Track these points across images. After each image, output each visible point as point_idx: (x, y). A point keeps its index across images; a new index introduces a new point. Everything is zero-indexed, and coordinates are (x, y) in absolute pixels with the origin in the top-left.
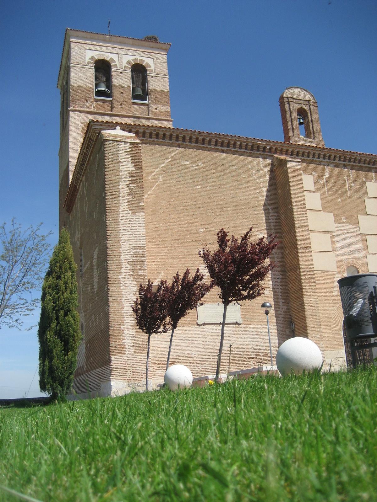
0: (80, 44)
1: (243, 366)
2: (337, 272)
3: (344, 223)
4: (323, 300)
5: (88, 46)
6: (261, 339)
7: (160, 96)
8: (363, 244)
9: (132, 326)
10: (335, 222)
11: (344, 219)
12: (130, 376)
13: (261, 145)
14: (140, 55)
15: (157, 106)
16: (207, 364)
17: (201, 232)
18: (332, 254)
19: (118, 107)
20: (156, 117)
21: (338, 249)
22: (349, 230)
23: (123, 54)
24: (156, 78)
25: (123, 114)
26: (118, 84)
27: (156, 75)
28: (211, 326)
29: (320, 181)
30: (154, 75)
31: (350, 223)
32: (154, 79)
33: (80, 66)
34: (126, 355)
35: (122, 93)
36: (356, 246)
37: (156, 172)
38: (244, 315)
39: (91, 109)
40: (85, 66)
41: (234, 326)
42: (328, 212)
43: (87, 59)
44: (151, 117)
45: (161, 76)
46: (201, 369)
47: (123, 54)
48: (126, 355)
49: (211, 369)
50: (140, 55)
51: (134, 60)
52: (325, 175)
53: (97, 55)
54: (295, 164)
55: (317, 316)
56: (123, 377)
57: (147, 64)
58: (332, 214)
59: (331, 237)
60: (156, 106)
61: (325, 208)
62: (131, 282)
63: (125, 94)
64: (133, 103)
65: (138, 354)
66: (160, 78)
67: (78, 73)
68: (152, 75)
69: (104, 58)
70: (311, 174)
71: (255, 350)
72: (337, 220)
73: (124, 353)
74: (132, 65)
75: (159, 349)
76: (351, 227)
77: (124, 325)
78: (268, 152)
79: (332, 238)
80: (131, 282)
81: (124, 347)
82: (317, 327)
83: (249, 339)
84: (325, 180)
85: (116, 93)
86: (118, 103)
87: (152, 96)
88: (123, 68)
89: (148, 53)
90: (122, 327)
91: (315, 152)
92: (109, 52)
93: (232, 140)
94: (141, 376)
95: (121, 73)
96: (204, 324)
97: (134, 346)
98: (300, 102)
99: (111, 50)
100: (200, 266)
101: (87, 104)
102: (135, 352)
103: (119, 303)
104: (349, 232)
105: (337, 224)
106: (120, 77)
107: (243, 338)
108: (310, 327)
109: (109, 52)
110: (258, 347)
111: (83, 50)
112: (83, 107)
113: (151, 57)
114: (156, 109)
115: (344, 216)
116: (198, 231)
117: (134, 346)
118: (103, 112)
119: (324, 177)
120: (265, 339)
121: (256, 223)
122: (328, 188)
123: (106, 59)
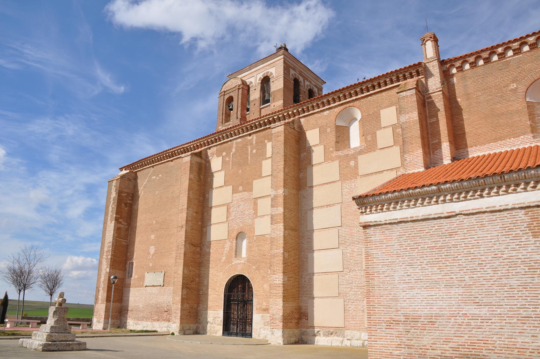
21: (232, 218)
27: (276, 79)
29: (227, 159)
51: (262, 76)
60: (274, 104)
76: (246, 194)
104: (244, 199)
115: (241, 185)
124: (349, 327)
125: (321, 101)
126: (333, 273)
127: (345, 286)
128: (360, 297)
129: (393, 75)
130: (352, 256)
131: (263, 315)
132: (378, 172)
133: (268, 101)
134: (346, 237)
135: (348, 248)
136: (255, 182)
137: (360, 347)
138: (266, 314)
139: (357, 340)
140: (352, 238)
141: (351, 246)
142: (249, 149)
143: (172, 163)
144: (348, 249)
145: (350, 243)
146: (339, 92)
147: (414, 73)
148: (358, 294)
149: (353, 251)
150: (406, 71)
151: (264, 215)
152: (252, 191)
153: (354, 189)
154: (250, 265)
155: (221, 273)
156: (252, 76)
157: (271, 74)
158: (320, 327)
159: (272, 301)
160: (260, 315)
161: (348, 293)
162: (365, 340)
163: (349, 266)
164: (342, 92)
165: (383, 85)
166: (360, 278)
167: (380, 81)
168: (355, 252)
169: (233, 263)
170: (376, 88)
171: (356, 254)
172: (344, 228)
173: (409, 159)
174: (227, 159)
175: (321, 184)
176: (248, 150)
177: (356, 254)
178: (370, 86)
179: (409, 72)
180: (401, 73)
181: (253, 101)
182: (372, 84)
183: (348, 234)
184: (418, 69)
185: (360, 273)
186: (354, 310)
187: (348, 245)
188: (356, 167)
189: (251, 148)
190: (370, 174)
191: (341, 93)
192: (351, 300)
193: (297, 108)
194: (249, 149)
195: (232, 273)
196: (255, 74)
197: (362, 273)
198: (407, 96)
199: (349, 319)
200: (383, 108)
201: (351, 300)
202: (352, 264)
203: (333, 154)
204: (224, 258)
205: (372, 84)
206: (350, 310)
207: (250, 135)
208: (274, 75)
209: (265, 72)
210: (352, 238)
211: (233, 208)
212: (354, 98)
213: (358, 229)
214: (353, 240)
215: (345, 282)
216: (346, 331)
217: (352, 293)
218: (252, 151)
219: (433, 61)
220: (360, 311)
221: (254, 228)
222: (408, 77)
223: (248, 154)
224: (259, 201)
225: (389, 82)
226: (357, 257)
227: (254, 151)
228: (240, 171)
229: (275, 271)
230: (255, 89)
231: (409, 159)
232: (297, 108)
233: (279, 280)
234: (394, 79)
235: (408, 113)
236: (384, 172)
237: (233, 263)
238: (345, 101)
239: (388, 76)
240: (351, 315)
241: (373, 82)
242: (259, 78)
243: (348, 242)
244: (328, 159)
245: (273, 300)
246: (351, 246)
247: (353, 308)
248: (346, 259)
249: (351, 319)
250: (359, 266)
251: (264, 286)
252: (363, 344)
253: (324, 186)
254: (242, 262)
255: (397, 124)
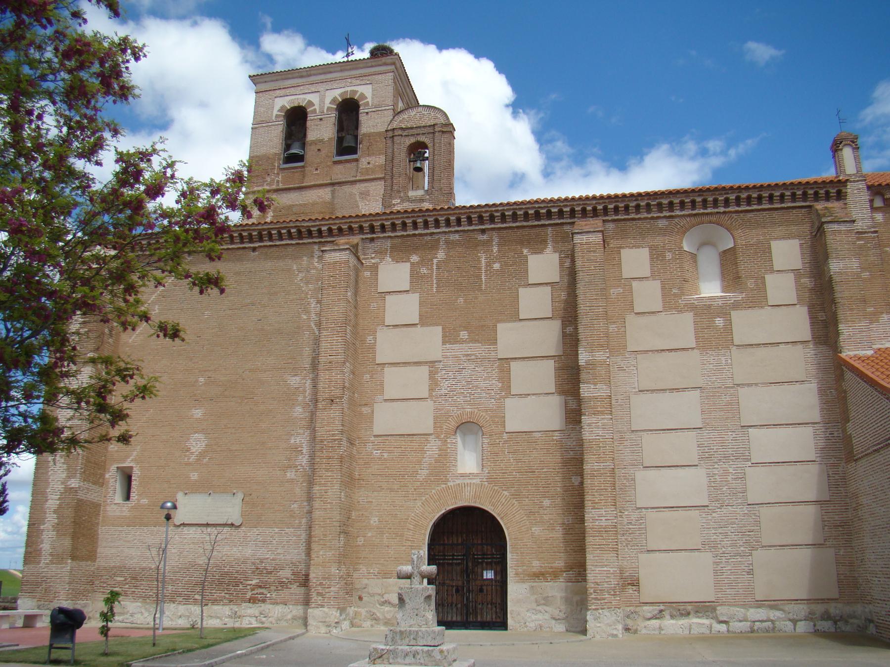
1: (235, 593)
2: (433, 436)
3: (463, 342)
4: (396, 487)
6: (270, 552)
7: (377, 141)
8: (500, 379)
9: (53, 526)
11: (464, 335)
12: (40, 595)
13: (312, 229)
14: (351, 85)
15: (370, 159)
16: (180, 585)
17: (201, 383)
18: (430, 403)
19: (312, 174)
21: (443, 391)
22: (472, 355)
24: (373, 113)
26: (314, 139)
27: (374, 110)
28: (194, 528)
29: (424, 271)
30: (370, 110)
31: (477, 341)
34: (41, 565)
35: (319, 150)
36: (482, 384)
37: (152, 300)
38: (248, 512)
39: (272, 185)
40: (270, 124)
41: (229, 529)
42: (431, 325)
43: (275, 112)
44: (360, 178)
45: (380, 109)
46: (170, 592)
48: (41, 565)
49: (185, 593)
50: (351, 85)
51: (341, 95)
53: (289, 102)
54: (338, 254)
55: (334, 520)
56: (34, 594)
58: (440, 328)
59: (430, 372)
60: (368, 159)
61: (425, 320)
62: (61, 465)
63: (324, 153)
64: (335, 163)
65: (54, 565)
66: (380, 112)
68: (366, 111)
70: (408, 260)
71: (257, 569)
72: (449, 338)
73: (39, 563)
75: (118, 558)
76: (478, 349)
77: (44, 524)
78: (308, 238)
79: (432, 375)
80: (61, 465)
81: (40, 555)
82: (330, 540)
83: (250, 552)
84: (435, 268)
85: (310, 153)
87: (365, 144)
88: (325, 111)
89: (364, 78)
90: (42, 527)
91: (414, 219)
93: (264, 230)
94: (53, 595)
96: (184, 525)
97: (51, 555)
98: (415, 131)
100: (192, 435)
101: (269, 179)
102: (52, 562)
103: (43, 494)
104: (473, 357)
105: (448, 346)
107: (240, 548)
108: (317, 539)
110: (263, 565)
112: (263, 185)
113: (368, 82)
114: (369, 163)
115: (466, 328)
116: (197, 381)
117: (51, 555)
119: (435, 261)
120: (276, 552)
121: (290, 361)
122: (438, 280)
123: (301, 104)
124: (724, 600)
125: (657, 201)
126: (687, 508)
127: (713, 532)
128: (742, 549)
129: (798, 189)
130: (726, 481)
131: (535, 584)
132: (770, 344)
133: (353, 150)
134: (712, 447)
135: (716, 466)
136: (500, 326)
137: (746, 632)
138: (540, 584)
139: (741, 621)
140: (724, 450)
141: (722, 463)
142: (483, 261)
143: (252, 253)
144: (717, 468)
145: (719, 458)
146: (684, 195)
147: (834, 193)
148: (738, 545)
149: (726, 472)
150: (821, 188)
151: (529, 395)
152: (496, 344)
153: (724, 367)
154: (496, 488)
155: (419, 503)
156: (313, 90)
157: (363, 96)
158: (666, 603)
159: (592, 558)
160: (526, 585)
161: (719, 542)
162: (754, 622)
163: (720, 498)
164: (702, 195)
165: (778, 200)
166: (743, 518)
167: (773, 192)
168: (730, 474)
169: (449, 484)
170: (764, 202)
171: (733, 477)
172: (707, 432)
173: (848, 333)
174: (424, 271)
175: (657, 351)
176: (480, 262)
177: (733, 477)
178: (755, 195)
179: (824, 190)
180: (812, 188)
181: (314, 143)
182: (758, 193)
183: (715, 442)
184: (841, 188)
185: (741, 510)
186: (733, 571)
187: (716, 461)
188: (728, 328)
189: (486, 259)
190: (755, 345)
191: (699, 196)
192: (726, 555)
193: (605, 203)
194: (483, 261)
195: (449, 503)
196: (322, 88)
197: (745, 509)
198: (840, 232)
199: (723, 588)
200: (776, 239)
201: (726, 555)
202: (726, 495)
203: (680, 301)
204: (425, 472)
205: (758, 193)
206: (724, 571)
207: (483, 231)
208: (369, 99)
209: (349, 89)
210: (724, 450)
211: (444, 372)
212: (722, 210)
213: (734, 436)
214: (725, 453)
215: (711, 523)
216: (718, 608)
217: (727, 542)
218: (489, 265)
219: (858, 181)
220: (744, 573)
221: (504, 417)
222: (833, 196)
223: (480, 269)
224: (514, 365)
225: (778, 198)
226: (734, 482)
227: (497, 266)
228: (461, 300)
229: (597, 503)
230: (321, 119)
231: (848, 333)
232: (605, 203)
233: (606, 520)
234: (798, 195)
235: (844, 259)
236: (781, 346)
237: (449, 484)
238: (702, 211)
239: (790, 188)
240: (726, 579)
241: (761, 191)
242: (332, 98)
243: (715, 456)
244: (671, 308)
245: (594, 557)
246: (722, 463)
247: (729, 568)
248: (713, 485)
249: (727, 587)
250: (739, 497)
251: (533, 529)
252: (752, 628)
253: (663, 353)
254: (474, 481)
255: (801, 271)
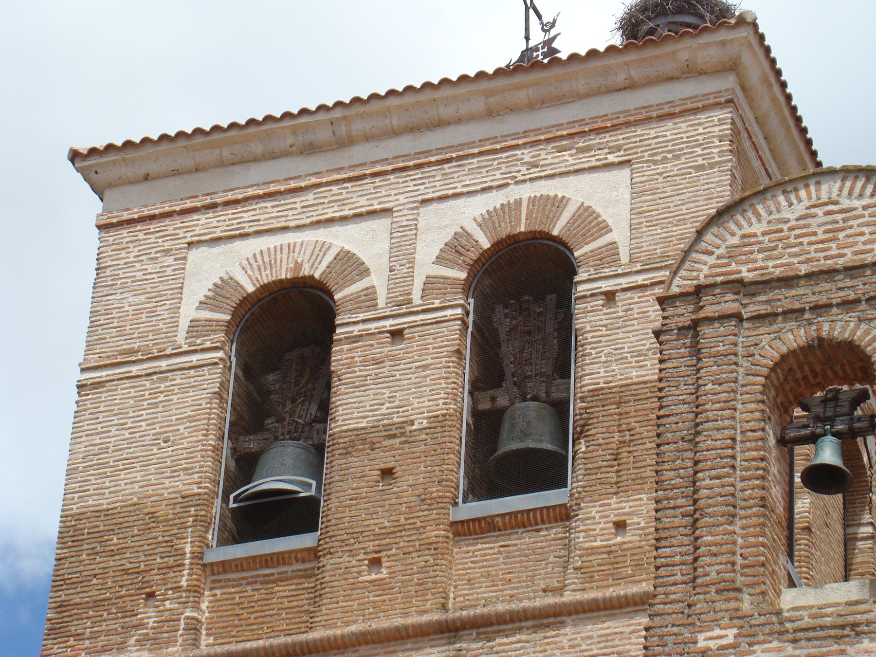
0: (153, 227)
5: (202, 219)
10: (373, 287)
14: (535, 172)
20: (610, 592)
23: (424, 202)
24: (636, 296)
25: (374, 625)
32: (619, 309)
33: (135, 369)
35: (387, 473)
44: (579, 596)
47: (424, 202)
50: (535, 172)
51: (487, 222)
52: (181, 646)
53: (249, 264)
57: (586, 215)
67: (423, 497)
68: (605, 286)
69: (298, 266)
74: (473, 255)
86: (352, 553)
92: (330, 221)
95: (397, 334)
99: (342, 203)
106: (385, 371)
109: (330, 221)
111: (170, 260)
113: (612, 158)
114: (620, 526)
118: (240, 646)
123: (306, 271)
